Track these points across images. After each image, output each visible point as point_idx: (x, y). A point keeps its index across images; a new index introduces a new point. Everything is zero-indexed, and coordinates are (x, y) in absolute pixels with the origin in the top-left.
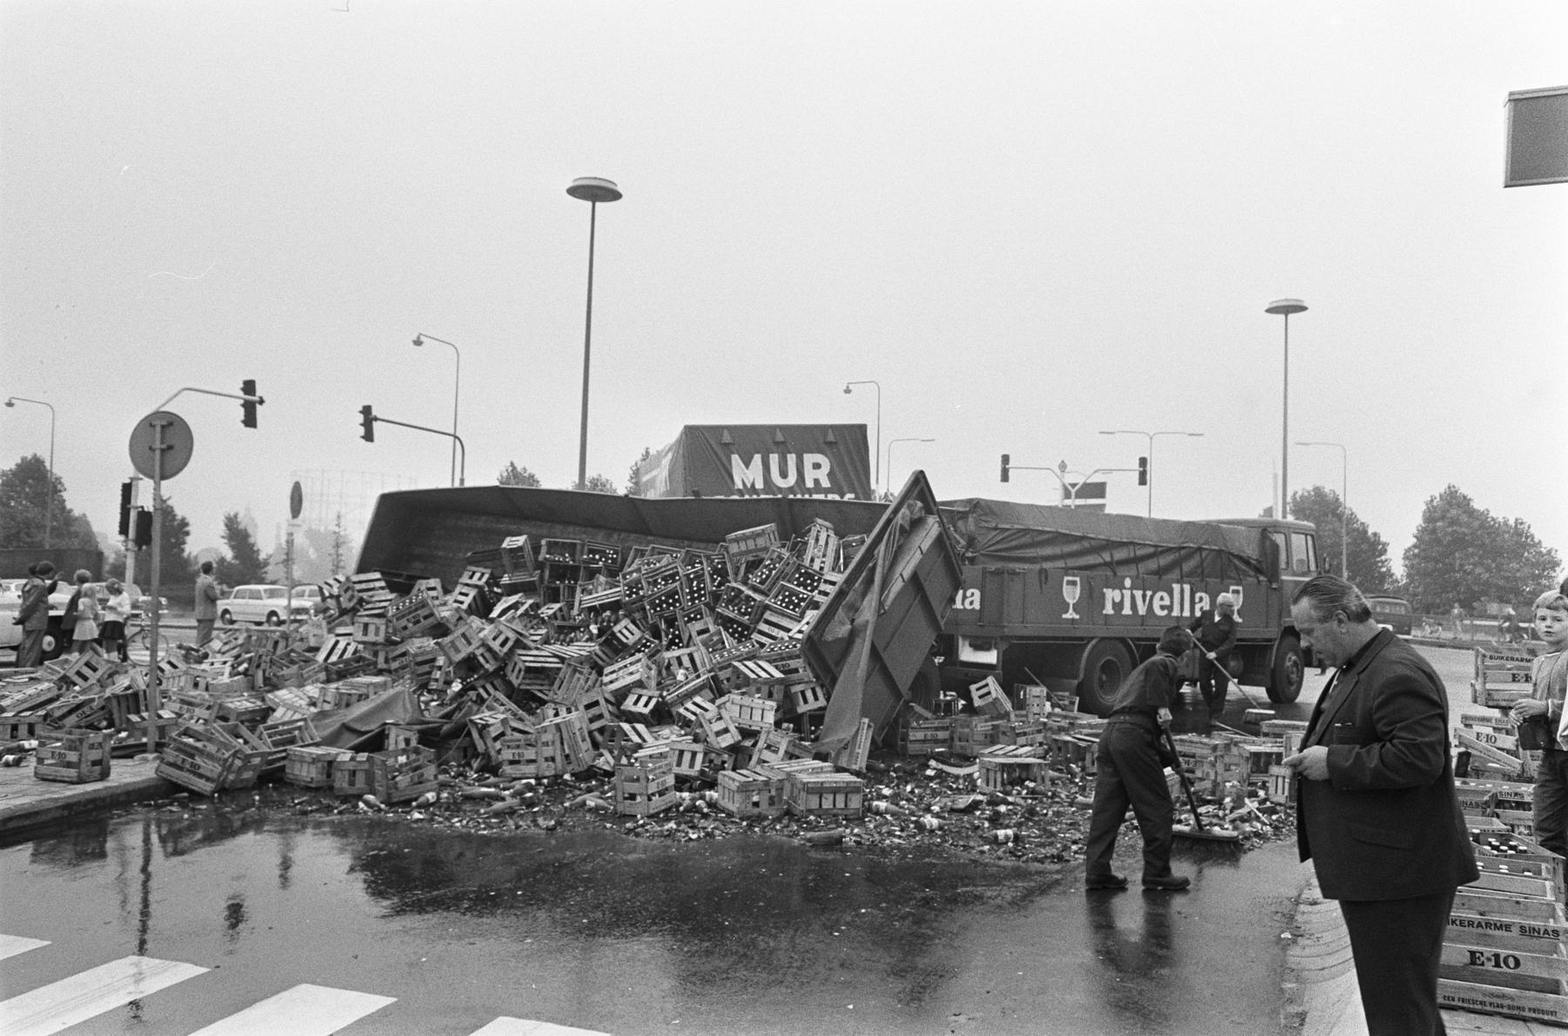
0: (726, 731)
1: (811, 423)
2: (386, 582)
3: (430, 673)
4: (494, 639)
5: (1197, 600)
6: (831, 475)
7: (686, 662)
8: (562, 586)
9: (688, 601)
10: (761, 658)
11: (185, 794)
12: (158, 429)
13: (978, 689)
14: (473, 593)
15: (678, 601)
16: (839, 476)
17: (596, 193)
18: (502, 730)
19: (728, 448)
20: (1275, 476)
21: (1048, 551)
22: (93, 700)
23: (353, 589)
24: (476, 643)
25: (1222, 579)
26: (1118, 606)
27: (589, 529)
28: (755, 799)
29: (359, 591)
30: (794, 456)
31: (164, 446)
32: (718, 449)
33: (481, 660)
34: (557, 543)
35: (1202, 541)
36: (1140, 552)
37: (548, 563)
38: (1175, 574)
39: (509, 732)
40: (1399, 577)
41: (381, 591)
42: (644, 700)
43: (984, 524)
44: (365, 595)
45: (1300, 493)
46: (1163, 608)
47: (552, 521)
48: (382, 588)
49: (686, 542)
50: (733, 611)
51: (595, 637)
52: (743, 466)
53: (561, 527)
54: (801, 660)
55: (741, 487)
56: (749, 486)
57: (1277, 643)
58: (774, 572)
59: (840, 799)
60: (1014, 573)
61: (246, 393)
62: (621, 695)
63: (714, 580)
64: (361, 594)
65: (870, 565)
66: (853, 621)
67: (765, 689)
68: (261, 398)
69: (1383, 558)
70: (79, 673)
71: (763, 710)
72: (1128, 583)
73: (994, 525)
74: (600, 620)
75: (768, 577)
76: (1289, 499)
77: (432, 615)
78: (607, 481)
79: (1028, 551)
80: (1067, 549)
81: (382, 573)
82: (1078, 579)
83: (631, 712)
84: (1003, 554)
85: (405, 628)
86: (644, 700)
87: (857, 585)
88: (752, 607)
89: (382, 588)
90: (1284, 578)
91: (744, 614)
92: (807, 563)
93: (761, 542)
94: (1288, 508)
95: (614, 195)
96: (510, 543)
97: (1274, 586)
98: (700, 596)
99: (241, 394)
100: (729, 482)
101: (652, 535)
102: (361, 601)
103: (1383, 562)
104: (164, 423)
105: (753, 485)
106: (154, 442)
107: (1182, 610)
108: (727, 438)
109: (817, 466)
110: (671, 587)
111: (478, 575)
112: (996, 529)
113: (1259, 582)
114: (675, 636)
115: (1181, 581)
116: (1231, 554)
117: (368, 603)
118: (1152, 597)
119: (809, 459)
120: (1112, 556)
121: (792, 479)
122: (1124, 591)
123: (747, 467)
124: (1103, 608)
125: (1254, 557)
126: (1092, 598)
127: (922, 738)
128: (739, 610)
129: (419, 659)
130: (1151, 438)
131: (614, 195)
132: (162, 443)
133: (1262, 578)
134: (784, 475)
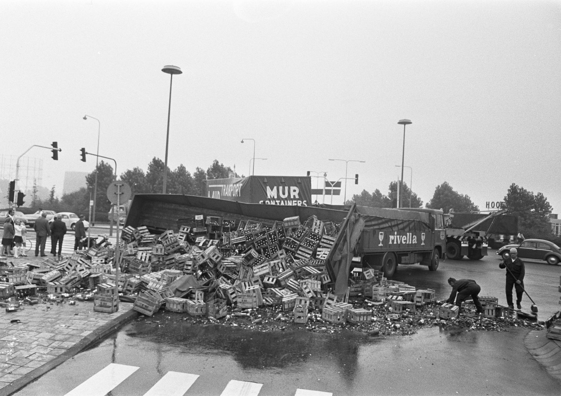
0: (310, 292)
2: (149, 229)
3: (184, 266)
4: (213, 256)
6: (299, 194)
9: (271, 242)
10: (310, 266)
11: (143, 316)
12: (119, 187)
14: (185, 236)
15: (267, 242)
17: (172, 71)
18: (233, 291)
19: (266, 184)
21: (373, 223)
22: (76, 278)
23: (139, 233)
24: (206, 258)
25: (420, 231)
26: (393, 241)
28: (339, 317)
30: (287, 187)
31: (121, 193)
33: (208, 263)
35: (415, 218)
36: (399, 222)
37: (211, 226)
39: (236, 292)
41: (147, 233)
42: (271, 279)
44: (143, 235)
45: (393, 183)
46: (404, 241)
47: (203, 208)
48: (147, 232)
49: (257, 218)
50: (289, 246)
52: (270, 190)
53: (206, 210)
54: (325, 267)
55: (270, 198)
56: (272, 197)
57: (433, 251)
58: (303, 234)
59: (365, 317)
61: (54, 147)
62: (262, 277)
63: (279, 235)
64: (142, 235)
65: (345, 235)
67: (316, 277)
68: (60, 149)
70: (67, 268)
71: (317, 284)
72: (396, 233)
74: (238, 248)
75: (301, 235)
77: (179, 245)
78: (141, 169)
81: (147, 226)
82: (383, 233)
83: (267, 283)
85: (169, 249)
86: (271, 279)
89: (147, 232)
91: (293, 248)
92: (313, 230)
93: (296, 223)
95: (179, 72)
97: (433, 232)
98: (275, 241)
99: (52, 147)
100: (266, 195)
101: (243, 215)
102: (142, 237)
104: (121, 185)
106: (117, 192)
108: (266, 181)
109: (295, 191)
111: (186, 229)
113: (429, 231)
114: (267, 255)
115: (409, 232)
117: (144, 238)
119: (292, 188)
120: (391, 224)
123: (272, 191)
124: (389, 242)
126: (386, 238)
128: (291, 246)
129: (180, 262)
131: (179, 72)
132: (120, 192)
133: (430, 230)
134: (284, 194)
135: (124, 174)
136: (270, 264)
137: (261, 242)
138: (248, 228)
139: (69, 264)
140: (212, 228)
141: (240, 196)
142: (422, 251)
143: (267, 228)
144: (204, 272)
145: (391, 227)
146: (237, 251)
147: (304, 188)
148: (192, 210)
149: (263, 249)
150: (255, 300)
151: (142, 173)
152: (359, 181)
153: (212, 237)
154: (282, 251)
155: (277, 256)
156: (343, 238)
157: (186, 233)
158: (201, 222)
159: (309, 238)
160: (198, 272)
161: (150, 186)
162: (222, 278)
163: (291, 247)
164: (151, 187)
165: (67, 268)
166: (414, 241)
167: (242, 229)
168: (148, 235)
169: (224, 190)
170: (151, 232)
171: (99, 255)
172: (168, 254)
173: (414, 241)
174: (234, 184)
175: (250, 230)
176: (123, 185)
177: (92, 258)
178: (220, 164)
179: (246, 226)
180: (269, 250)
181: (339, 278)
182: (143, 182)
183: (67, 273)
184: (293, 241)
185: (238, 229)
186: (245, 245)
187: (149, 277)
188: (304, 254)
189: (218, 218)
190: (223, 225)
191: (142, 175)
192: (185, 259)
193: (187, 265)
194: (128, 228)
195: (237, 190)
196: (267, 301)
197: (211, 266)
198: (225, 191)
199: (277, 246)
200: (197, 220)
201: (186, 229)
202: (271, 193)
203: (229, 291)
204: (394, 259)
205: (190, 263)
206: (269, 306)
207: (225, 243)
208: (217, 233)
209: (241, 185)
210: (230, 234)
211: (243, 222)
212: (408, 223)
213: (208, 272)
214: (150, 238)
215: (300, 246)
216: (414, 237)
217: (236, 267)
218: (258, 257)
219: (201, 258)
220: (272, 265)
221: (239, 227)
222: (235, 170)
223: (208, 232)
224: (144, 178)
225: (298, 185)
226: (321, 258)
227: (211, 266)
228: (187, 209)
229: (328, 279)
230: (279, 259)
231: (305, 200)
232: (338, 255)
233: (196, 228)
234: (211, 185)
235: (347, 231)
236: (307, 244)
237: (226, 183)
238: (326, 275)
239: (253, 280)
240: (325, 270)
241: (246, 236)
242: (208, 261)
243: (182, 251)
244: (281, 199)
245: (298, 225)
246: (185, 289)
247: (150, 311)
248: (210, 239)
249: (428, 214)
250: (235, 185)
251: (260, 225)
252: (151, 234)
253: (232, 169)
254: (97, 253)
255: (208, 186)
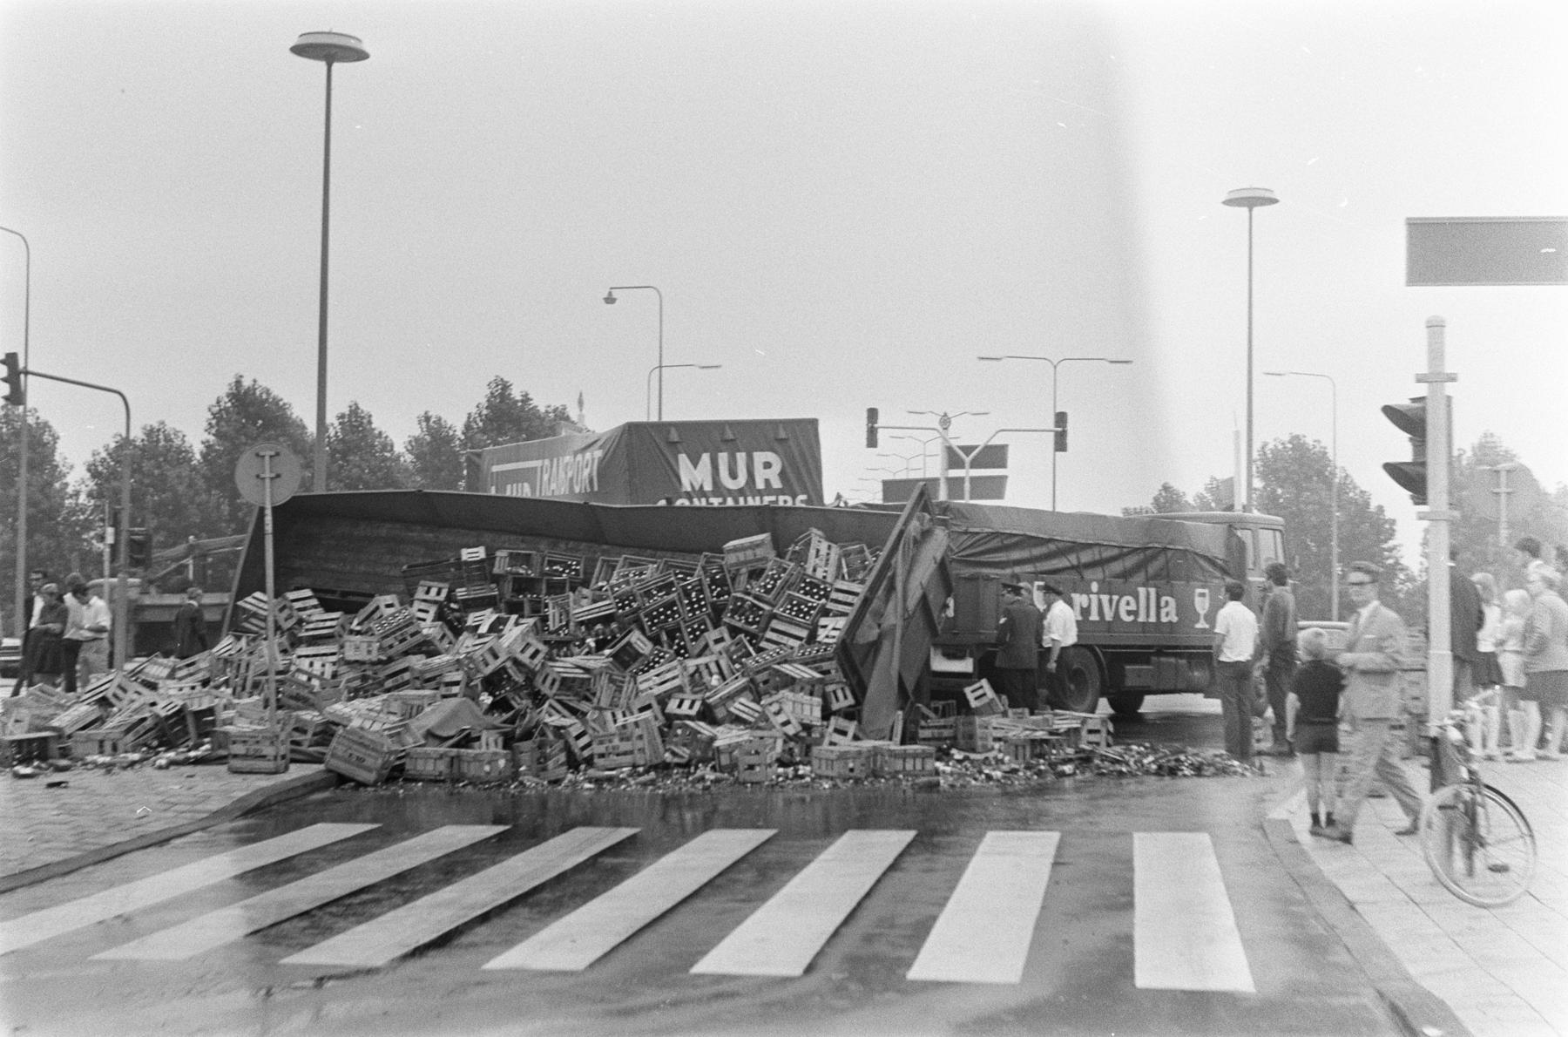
1: (751, 418)
2: (319, 599)
4: (522, 651)
5: (1163, 604)
6: (783, 475)
7: (714, 668)
8: (525, 599)
10: (795, 661)
11: (352, 784)
12: (267, 458)
13: (973, 691)
14: (433, 610)
15: (677, 612)
16: (792, 477)
18: (583, 729)
20: (1237, 434)
21: (1016, 555)
22: (144, 720)
23: (291, 608)
25: (1188, 582)
27: (528, 538)
28: (851, 765)
29: (300, 610)
31: (273, 475)
32: (662, 445)
34: (519, 554)
36: (1107, 554)
37: (510, 577)
38: (1140, 577)
40: (1416, 573)
42: (687, 704)
43: (956, 529)
44: (304, 615)
45: (1271, 446)
46: (1129, 613)
48: (315, 607)
50: (740, 620)
51: (593, 650)
53: (491, 536)
54: (834, 662)
55: (689, 489)
58: (779, 582)
60: (988, 579)
62: (663, 700)
63: (712, 591)
64: (301, 613)
65: (889, 574)
66: (879, 626)
67: (808, 688)
69: (1391, 543)
72: (1095, 587)
73: (963, 529)
74: (593, 633)
75: (774, 586)
76: (1255, 455)
78: (176, 433)
79: (997, 555)
80: (1037, 552)
81: (314, 590)
84: (972, 559)
85: (391, 646)
86: (687, 704)
87: (880, 592)
88: (760, 616)
89: (315, 607)
90: (1250, 579)
91: (751, 624)
92: (809, 572)
93: (760, 552)
94: (1254, 469)
95: (361, 55)
96: (466, 554)
98: (701, 607)
101: (607, 543)
102: (300, 622)
103: (1391, 550)
104: (273, 453)
105: (701, 487)
107: (1148, 616)
108: (674, 436)
109: (767, 465)
110: (667, 598)
111: (434, 591)
112: (966, 533)
114: (681, 647)
116: (1196, 554)
117: (308, 623)
118: (1118, 602)
119: (760, 457)
120: (1078, 558)
121: (742, 479)
122: (1091, 596)
125: (1221, 557)
127: (930, 736)
128: (747, 618)
129: (428, 676)
130: (1055, 367)
131: (361, 55)
132: (271, 472)
134: (734, 475)
135: (104, 455)
136: (685, 668)
137: (662, 613)
138: (623, 576)
139: (120, 687)
140: (514, 585)
141: (596, 489)
142: (1199, 648)
143: (680, 576)
144: (498, 698)
145: (1076, 568)
146: (591, 642)
147: (798, 459)
148: (446, 536)
149: (668, 634)
150: (639, 744)
151: (179, 447)
152: (1070, 439)
153: (515, 608)
154: (721, 633)
155: (706, 646)
156: (885, 583)
157: (435, 602)
158: (478, 569)
159: (798, 592)
160: (482, 698)
161: (218, 506)
162: (551, 706)
163: (747, 623)
164: (225, 509)
165: (115, 696)
166: (1167, 614)
167: (605, 583)
168: (318, 615)
169: (546, 477)
170: (328, 606)
171: (180, 674)
172: (390, 660)
173: (1167, 614)
174: (575, 454)
175: (627, 583)
176: (278, 454)
177: (160, 685)
178: (516, 394)
179: (615, 573)
180: (685, 634)
181: (873, 688)
182: (190, 486)
183: (115, 709)
184: (754, 605)
185: (593, 586)
186: (614, 625)
187: (347, 710)
188: (785, 639)
189: (530, 555)
190: (547, 574)
191: (180, 456)
192: (440, 666)
193: (449, 684)
194: (254, 598)
195: (586, 472)
196: (674, 754)
197: (519, 678)
198: (549, 480)
199: (708, 622)
200: (466, 563)
201: (433, 591)
202: (693, 474)
203: (571, 729)
204: (1094, 666)
205: (458, 676)
206: (678, 765)
207: (556, 627)
208: (531, 601)
209: (598, 454)
210: (568, 597)
211: (608, 561)
212: (1142, 556)
213: (510, 695)
214: (328, 624)
215: (774, 616)
216: (1167, 603)
217: (589, 679)
218: (651, 653)
219: (489, 658)
220: (692, 670)
221: (594, 581)
222: (581, 417)
223: (501, 595)
224: (194, 469)
225: (779, 450)
226: (827, 641)
227: (517, 679)
228: (431, 535)
229: (846, 697)
230: (712, 653)
231: (803, 493)
232: (870, 627)
233: (464, 589)
234: (498, 464)
235: (896, 562)
236: (791, 610)
237: (551, 453)
238: (841, 686)
239: (637, 704)
240: (837, 671)
241: (615, 598)
242: (509, 664)
243: (427, 648)
244: (725, 492)
245: (765, 559)
246: (452, 733)
247: (369, 770)
248: (511, 612)
249: (1221, 529)
250: (579, 457)
251: (658, 567)
252: (328, 610)
253: (573, 413)
254: (174, 670)
255: (489, 469)
